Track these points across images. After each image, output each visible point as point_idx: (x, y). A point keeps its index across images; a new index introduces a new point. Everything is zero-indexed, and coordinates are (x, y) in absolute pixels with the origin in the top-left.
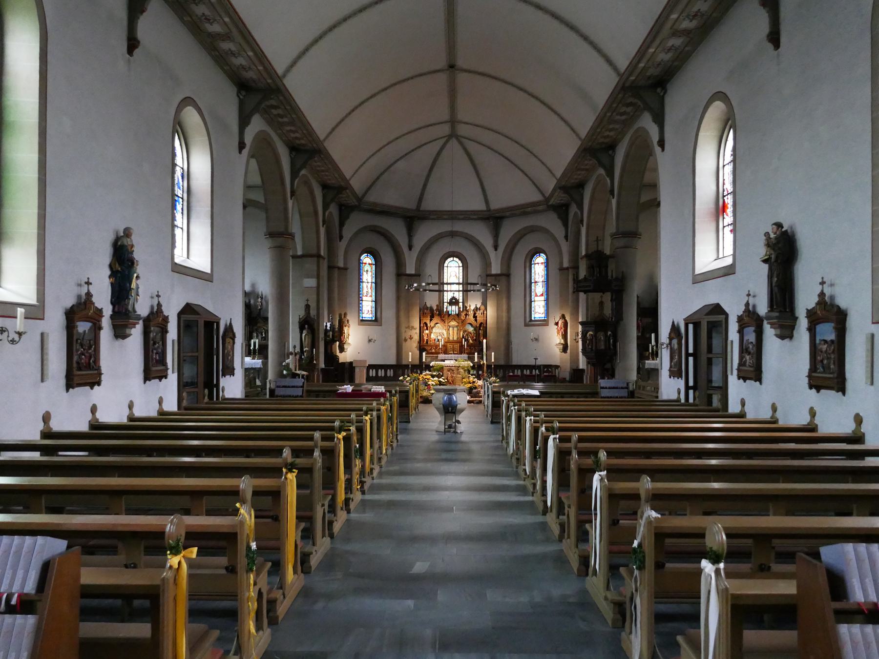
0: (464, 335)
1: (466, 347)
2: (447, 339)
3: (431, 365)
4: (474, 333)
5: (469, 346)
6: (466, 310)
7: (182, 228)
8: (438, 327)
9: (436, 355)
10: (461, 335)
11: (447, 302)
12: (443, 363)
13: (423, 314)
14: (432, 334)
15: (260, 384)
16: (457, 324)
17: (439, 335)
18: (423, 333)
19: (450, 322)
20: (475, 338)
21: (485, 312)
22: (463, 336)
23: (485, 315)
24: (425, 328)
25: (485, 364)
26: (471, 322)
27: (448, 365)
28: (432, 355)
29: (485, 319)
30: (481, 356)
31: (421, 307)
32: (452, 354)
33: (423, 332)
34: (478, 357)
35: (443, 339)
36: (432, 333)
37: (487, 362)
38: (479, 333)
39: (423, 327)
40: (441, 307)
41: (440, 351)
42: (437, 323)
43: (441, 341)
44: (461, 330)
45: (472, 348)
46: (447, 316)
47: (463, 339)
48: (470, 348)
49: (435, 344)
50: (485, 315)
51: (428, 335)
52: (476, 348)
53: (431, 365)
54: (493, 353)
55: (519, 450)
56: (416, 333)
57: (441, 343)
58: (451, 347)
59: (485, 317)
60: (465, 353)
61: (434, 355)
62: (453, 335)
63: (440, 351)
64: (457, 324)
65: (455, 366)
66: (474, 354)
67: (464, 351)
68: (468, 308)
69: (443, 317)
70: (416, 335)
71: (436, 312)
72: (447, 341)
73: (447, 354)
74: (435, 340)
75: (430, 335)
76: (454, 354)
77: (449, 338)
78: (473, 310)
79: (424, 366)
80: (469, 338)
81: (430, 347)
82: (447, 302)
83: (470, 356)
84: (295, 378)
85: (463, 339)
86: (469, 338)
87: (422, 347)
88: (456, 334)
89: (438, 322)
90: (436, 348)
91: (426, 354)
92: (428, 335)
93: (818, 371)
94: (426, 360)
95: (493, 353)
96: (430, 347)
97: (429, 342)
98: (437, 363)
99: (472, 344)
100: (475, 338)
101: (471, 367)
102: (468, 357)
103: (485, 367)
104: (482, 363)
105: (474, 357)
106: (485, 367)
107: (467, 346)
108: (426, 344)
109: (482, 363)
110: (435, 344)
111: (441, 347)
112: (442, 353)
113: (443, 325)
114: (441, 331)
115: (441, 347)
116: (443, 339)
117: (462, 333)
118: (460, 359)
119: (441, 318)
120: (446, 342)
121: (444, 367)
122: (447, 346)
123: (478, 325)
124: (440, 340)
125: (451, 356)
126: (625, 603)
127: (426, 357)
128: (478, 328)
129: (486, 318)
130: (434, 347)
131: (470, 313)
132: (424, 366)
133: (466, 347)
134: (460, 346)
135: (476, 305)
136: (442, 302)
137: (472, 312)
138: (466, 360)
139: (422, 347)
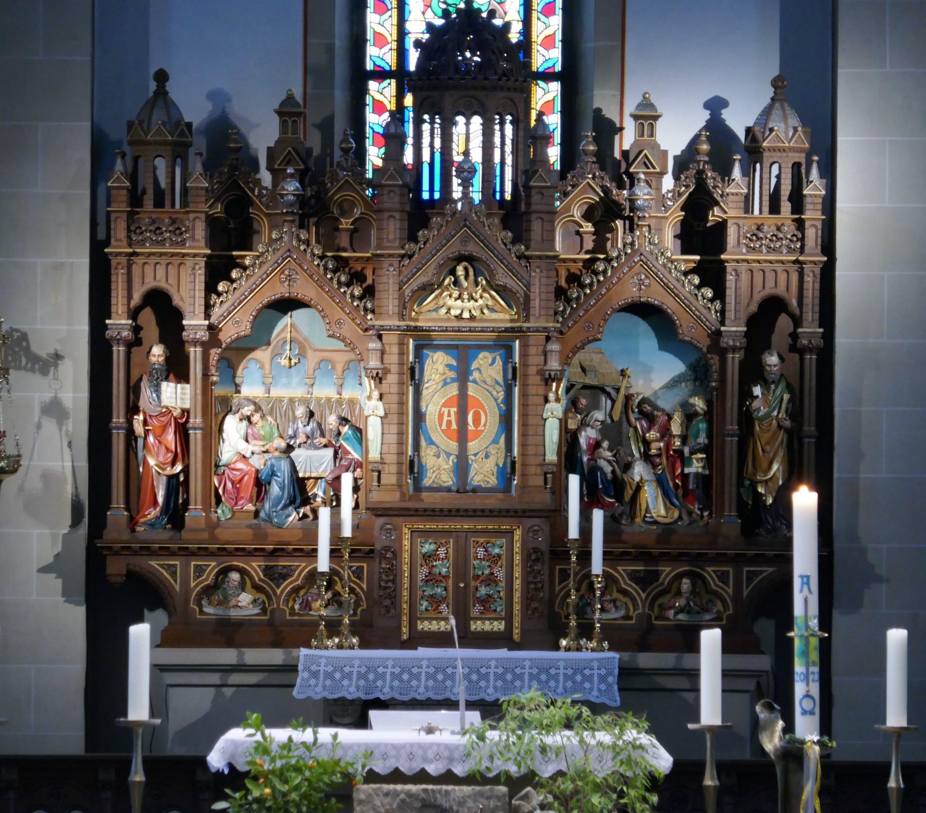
0: (586, 437)
1: (597, 566)
2: (389, 478)
3: (216, 759)
4: (690, 416)
5: (644, 556)
6: (604, 157)
7: (704, 298)
8: (301, 347)
9: (275, 656)
10: (552, 433)
11: (400, 74)
12: (348, 735)
13: (135, 199)
14: (233, 427)
15: (213, 295)
16: (503, 317)
17: (303, 429)
18: (133, 409)
19: (426, 289)
20: (696, 467)
21: (814, 188)
22: (569, 439)
23: (813, 215)
24: (158, 352)
25: (814, 752)
26: (657, 296)
27: (406, 768)
28: (228, 656)
29: (814, 257)
30: (763, 662)
31: (117, 132)
32: (442, 640)
33: (133, 391)
34: (727, 674)
35: (347, 481)
36: (227, 407)
37: (826, 728)
38: (747, 420)
39: (135, 341)
40: (326, 127)
41: (320, 609)
42: (286, 305)
43: (335, 502)
44: (548, 380)
45: (667, 571)
46: (393, 228)
47: (574, 481)
48: (644, 580)
49: (260, 534)
50: (813, 215)
51: (183, 431)
52: (710, 572)
53: (216, 759)
54: (896, 637)
55: (418, 122)
56: (55, 410)
57: (324, 514)
58: (442, 568)
59: (812, 235)
60: (586, 631)
61: (254, 656)
62: (462, 436)
63: (320, 609)
64: (503, 317)
65: (469, 779)
66: (693, 646)
67: (583, 610)
68: (627, 139)
69: (358, 233)
70: (50, 425)
71: (278, 175)
72: (391, 498)
73: (391, 640)
74: (261, 485)
75: (214, 433)
76: (470, 639)
77: (414, 468)
78: (682, 164)
79: (138, 776)
80: (639, 471)
81: (212, 566)
82: (400, 74)
83: (646, 660)
84: (141, 338)
85: (574, 481)
86: (639, 471)
87: (116, 568)
88: (490, 421)
89: (304, 289)
90: (276, 576)
91: (163, 640)
92: (183, 431)
93: (468, 213)
94: (158, 704)
95: (896, 637)
96: (212, 566)
97: (195, 513)
98: (279, 735)
99: (667, 531)
100: (696, 467)
101: (654, 782)
102: (626, 673)
103: (810, 789)
104: (772, 742)
105: (694, 675)
106: (810, 789)
107: (607, 556)
108: (163, 535)
109: (772, 742)
110: (260, 534)
111: (323, 564)
112: (333, 628)
113: (349, 329)
114: (325, 391)
115: (323, 564)
116: (347, 481)
117: (554, 410)
118: (532, 695)
119: (328, 240)
120: (379, 511)
121: (363, 790)
122: (391, 554)
123: (735, 328)
124: (319, 491)
125: (441, 667)
126: (529, 322)
127: (158, 669)
128: (734, 359)
129: (828, 246)
130: (255, 567)
131: (642, 193)
132: (138, 776)
133: (597, 566)
134: (532, 556)
135: (715, 105)
136: (341, 69)
137: (668, 182)
138: (597, 709)
139: (116, 568)
